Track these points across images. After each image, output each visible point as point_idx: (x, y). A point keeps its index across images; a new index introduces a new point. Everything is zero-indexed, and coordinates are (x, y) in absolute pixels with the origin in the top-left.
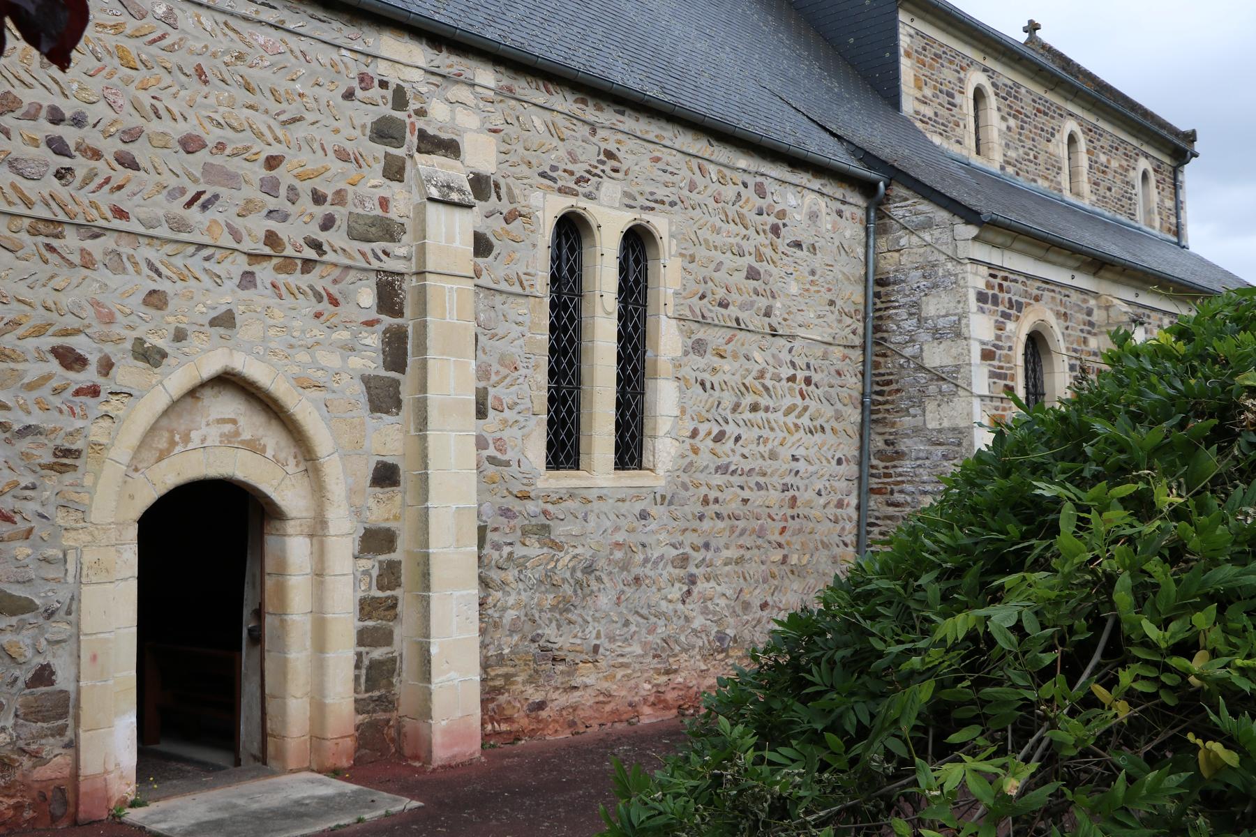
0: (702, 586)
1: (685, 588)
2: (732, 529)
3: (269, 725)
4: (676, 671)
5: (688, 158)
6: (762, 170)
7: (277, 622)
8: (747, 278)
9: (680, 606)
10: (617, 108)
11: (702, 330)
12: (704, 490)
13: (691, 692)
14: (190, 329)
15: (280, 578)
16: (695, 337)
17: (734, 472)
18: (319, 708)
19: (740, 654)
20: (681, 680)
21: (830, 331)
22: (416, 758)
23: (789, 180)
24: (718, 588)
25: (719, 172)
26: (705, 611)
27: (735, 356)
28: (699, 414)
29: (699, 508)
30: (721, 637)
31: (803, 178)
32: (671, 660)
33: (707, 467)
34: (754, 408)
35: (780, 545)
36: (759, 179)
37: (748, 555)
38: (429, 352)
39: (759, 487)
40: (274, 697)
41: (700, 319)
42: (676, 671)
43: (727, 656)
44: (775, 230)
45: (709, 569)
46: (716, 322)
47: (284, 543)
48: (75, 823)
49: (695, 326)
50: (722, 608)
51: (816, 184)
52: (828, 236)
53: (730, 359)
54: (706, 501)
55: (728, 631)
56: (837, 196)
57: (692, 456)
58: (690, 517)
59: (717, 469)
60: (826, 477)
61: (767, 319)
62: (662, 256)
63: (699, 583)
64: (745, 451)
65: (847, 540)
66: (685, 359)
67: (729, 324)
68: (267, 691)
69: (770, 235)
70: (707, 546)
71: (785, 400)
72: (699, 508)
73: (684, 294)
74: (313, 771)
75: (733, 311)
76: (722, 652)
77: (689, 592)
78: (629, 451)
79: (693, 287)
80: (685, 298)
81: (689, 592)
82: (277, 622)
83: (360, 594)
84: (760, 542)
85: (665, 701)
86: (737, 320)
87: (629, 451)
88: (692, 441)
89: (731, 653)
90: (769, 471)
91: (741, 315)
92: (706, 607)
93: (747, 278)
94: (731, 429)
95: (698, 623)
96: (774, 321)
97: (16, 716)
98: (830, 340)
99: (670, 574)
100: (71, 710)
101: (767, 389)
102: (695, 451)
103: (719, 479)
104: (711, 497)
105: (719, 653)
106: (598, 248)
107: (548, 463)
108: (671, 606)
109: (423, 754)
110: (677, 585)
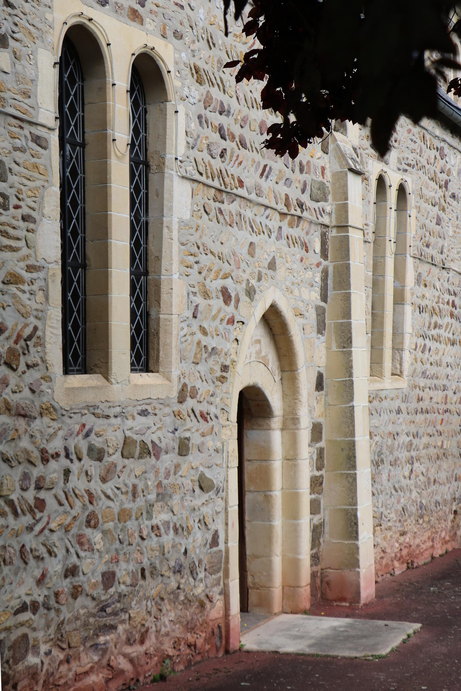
3: (249, 579)
7: (260, 498)
15: (264, 463)
18: (292, 565)
22: (343, 599)
38: (352, 287)
40: (256, 557)
47: (269, 436)
48: (227, 652)
62: (409, 208)
68: (248, 552)
74: (286, 613)
78: (144, 356)
82: (260, 498)
83: (311, 474)
87: (144, 356)
97: (205, 570)
100: (223, 566)
106: (388, 203)
107: (132, 364)
109: (349, 596)
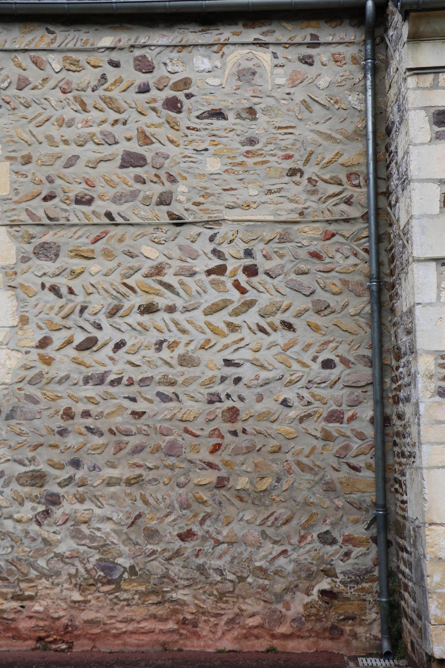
0: (67, 507)
1: (41, 508)
2: (119, 448)
4: (31, 598)
5: (13, 55)
6: (142, 41)
8: (122, 166)
9: (34, 527)
10: (110, 26)
11: (51, 233)
12: (64, 404)
13: (58, 623)
14: (34, 159)
16: (36, 242)
17: (113, 383)
19: (142, 588)
20: (41, 609)
21: (293, 206)
23: (200, 42)
24: (98, 511)
25: (65, 59)
26: (77, 535)
27: (108, 255)
28: (50, 323)
29: (58, 423)
30: (108, 567)
31: (226, 33)
32: (23, 585)
33: (67, 377)
34: (149, 309)
35: (211, 465)
36: (138, 53)
37: (148, 475)
39: (163, 398)
41: (46, 221)
42: (31, 598)
43: (118, 589)
44: (173, 105)
45: (81, 489)
46: (76, 221)
49: (32, 230)
50: (108, 534)
51: (253, 34)
52: (279, 93)
53: (101, 259)
54: (68, 414)
55: (120, 561)
56: (298, 40)
57: (42, 367)
58: (44, 432)
59: (86, 380)
60: (303, 382)
61: (165, 208)
63: (64, 503)
64: (134, 359)
65: (359, 462)
66: (25, 266)
67: (96, 221)
69: (166, 112)
70: (76, 464)
71: (206, 297)
72: (58, 423)
73: (16, 198)
75: (100, 206)
76: (109, 582)
77: (47, 513)
79: (28, 188)
80: (17, 202)
81: (47, 513)
84: (171, 461)
85: (16, 629)
86: (109, 215)
88: (41, 351)
89: (124, 586)
90: (180, 380)
91: (114, 209)
92: (80, 532)
93: (122, 166)
94: (108, 334)
95: (66, 546)
96: (177, 208)
98: (295, 217)
99: (16, 492)
101: (169, 287)
102: (48, 361)
103: (91, 391)
104: (78, 408)
105: (103, 584)
108: (19, 527)
110: (28, 505)
